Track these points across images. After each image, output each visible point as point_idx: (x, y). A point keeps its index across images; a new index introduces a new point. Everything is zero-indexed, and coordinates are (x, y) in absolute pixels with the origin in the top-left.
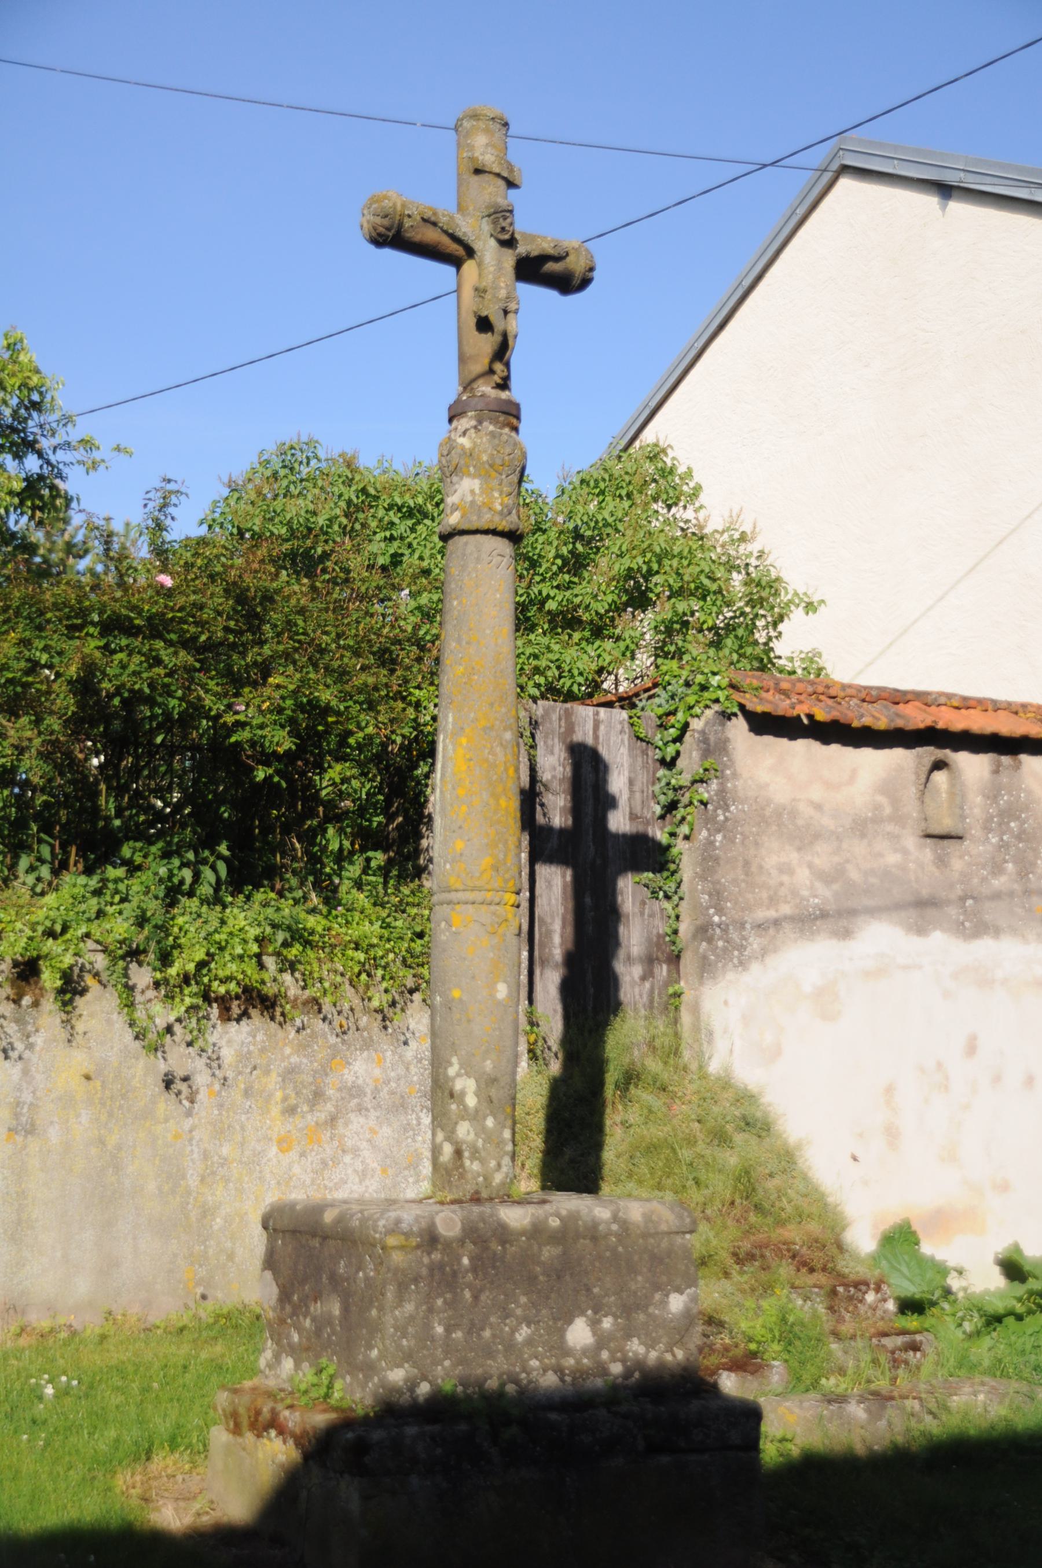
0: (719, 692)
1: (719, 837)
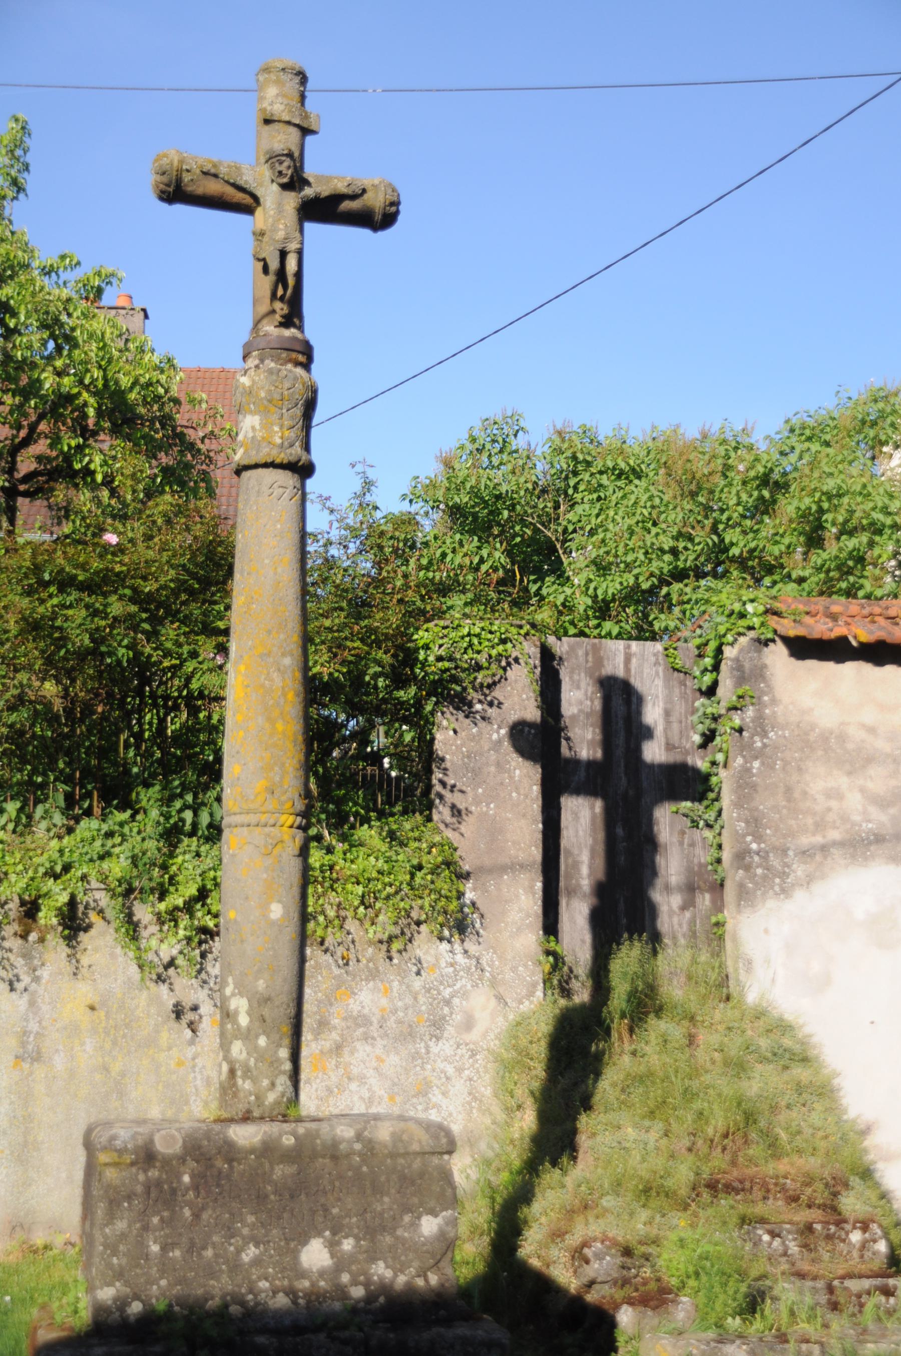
0: (755, 619)
1: (756, 764)
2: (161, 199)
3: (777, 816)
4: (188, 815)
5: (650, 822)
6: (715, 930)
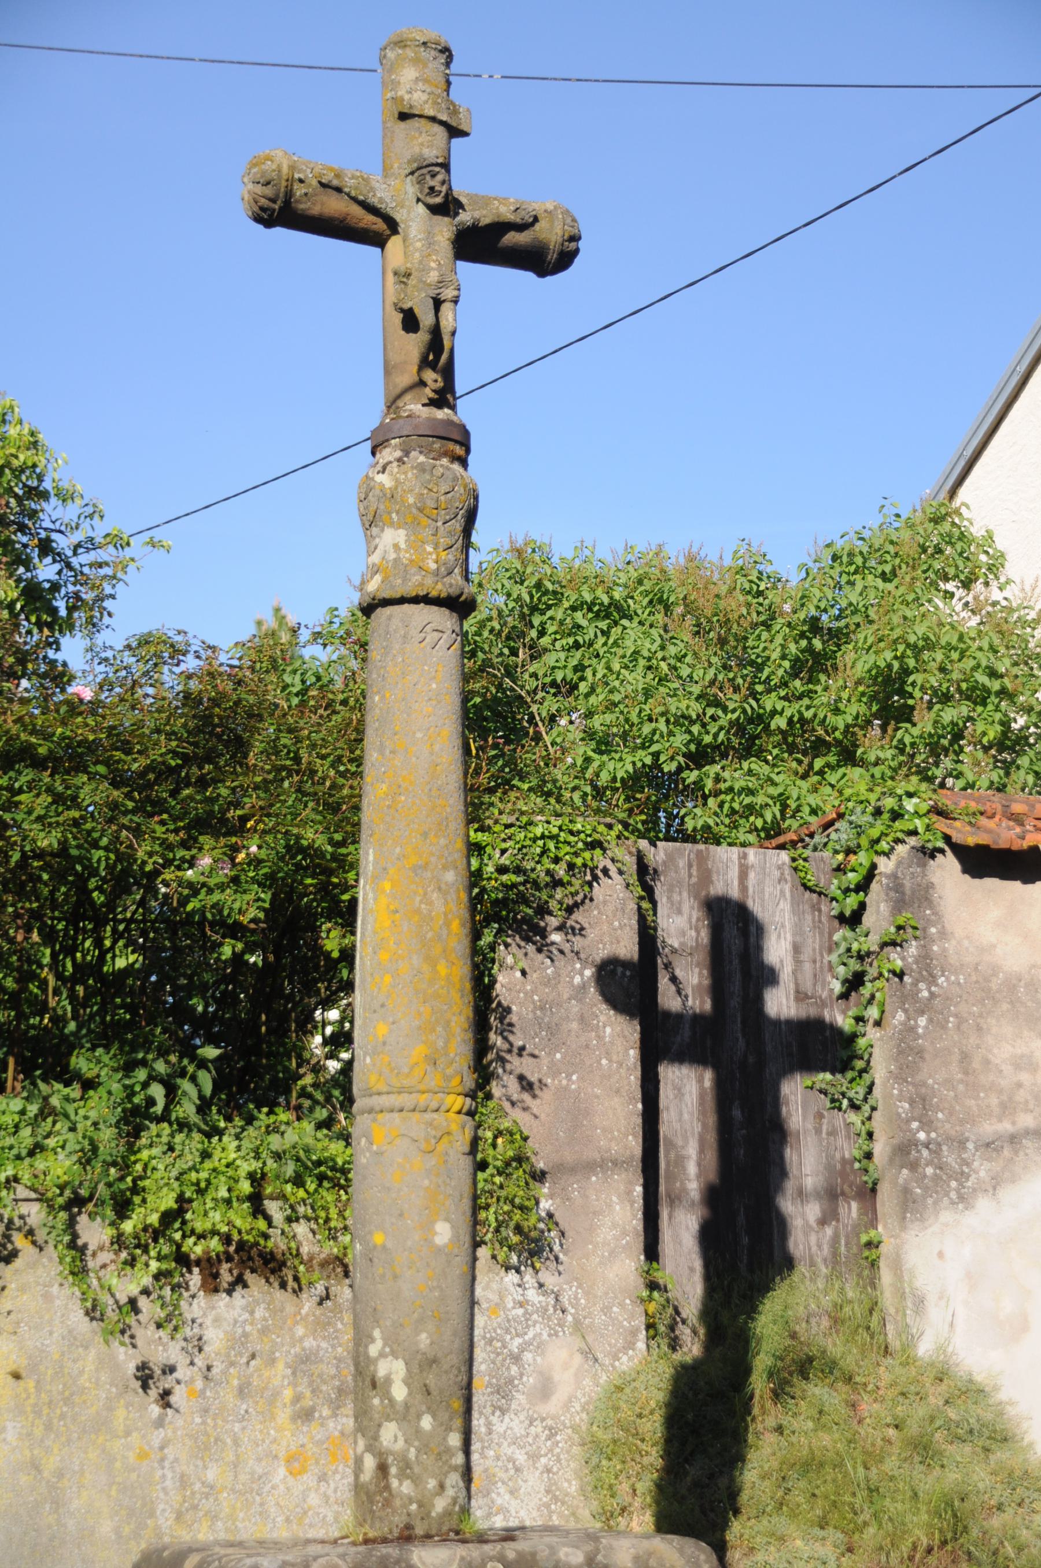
0: (917, 821)
1: (922, 1021)
2: (258, 219)
3: (952, 1093)
4: (157, 1091)
5: (775, 1101)
6: (866, 1253)
